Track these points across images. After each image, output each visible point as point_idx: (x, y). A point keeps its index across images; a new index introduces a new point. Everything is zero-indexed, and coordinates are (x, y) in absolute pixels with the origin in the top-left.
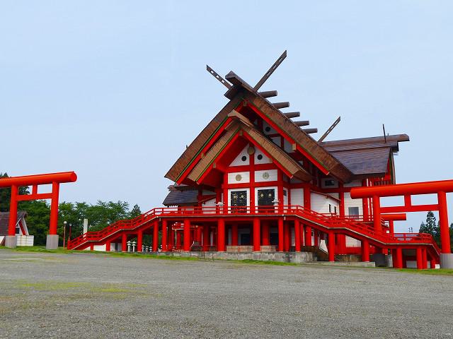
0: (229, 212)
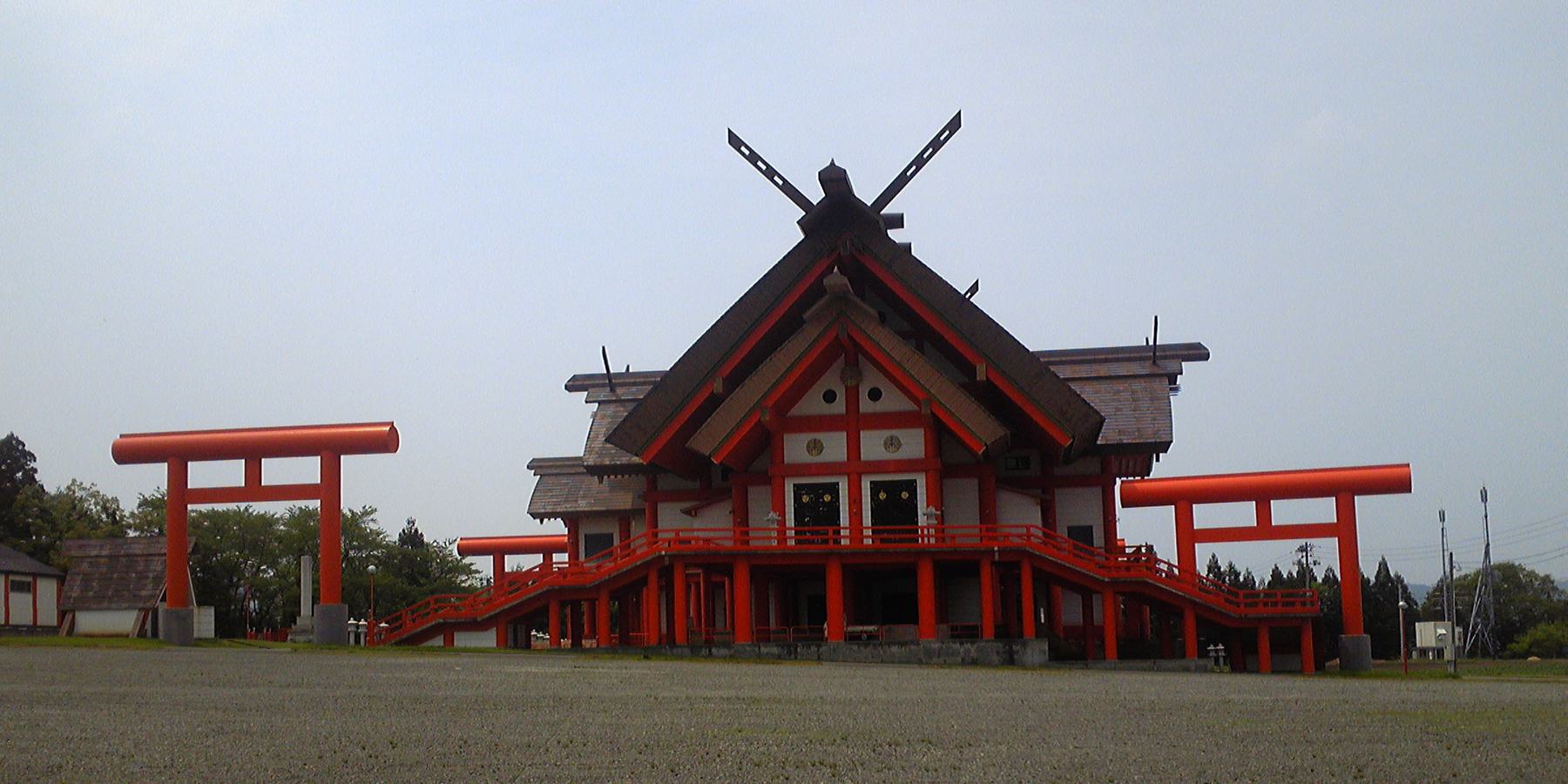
0: (792, 543)
